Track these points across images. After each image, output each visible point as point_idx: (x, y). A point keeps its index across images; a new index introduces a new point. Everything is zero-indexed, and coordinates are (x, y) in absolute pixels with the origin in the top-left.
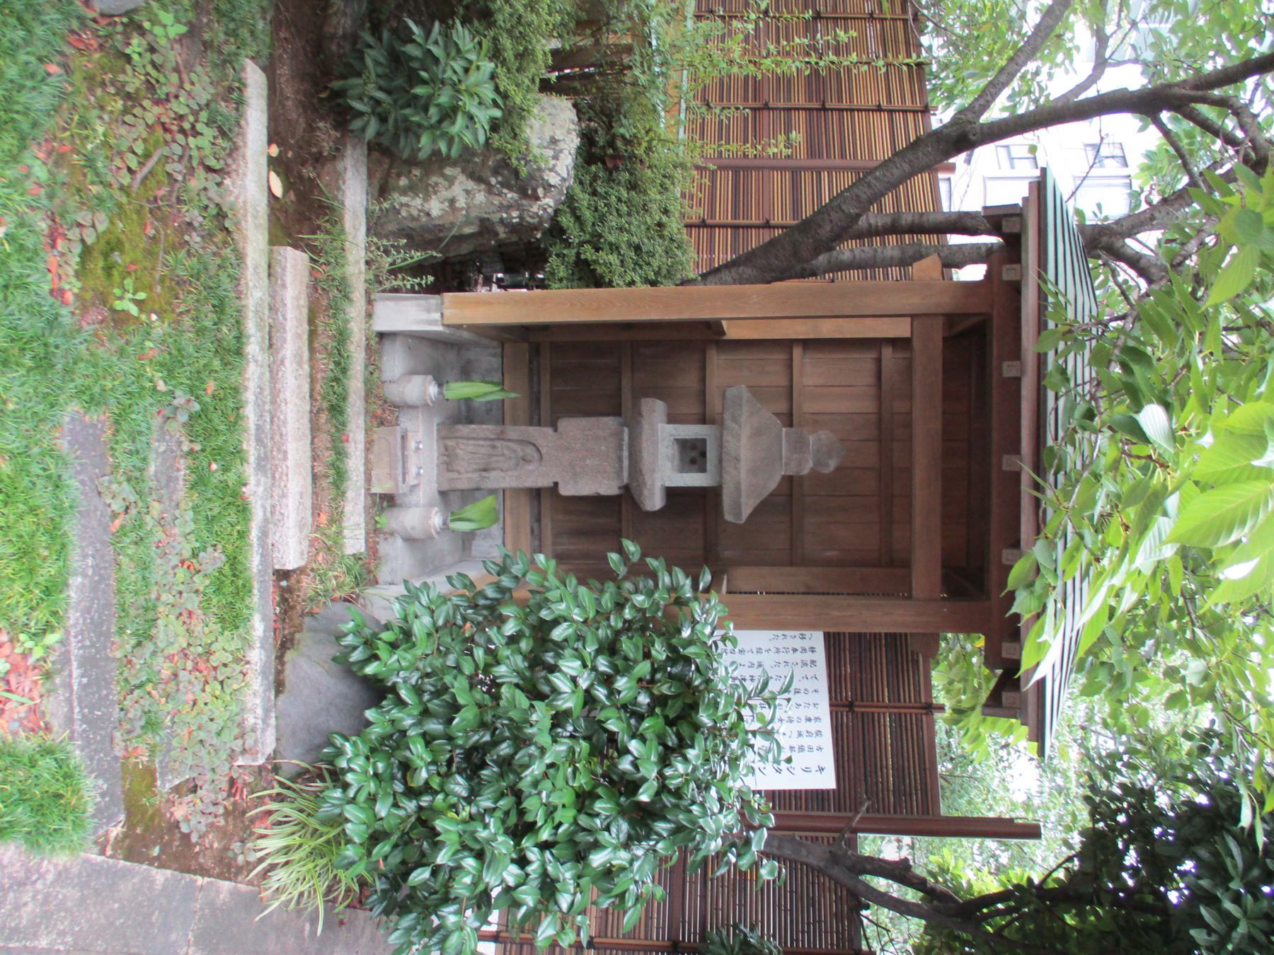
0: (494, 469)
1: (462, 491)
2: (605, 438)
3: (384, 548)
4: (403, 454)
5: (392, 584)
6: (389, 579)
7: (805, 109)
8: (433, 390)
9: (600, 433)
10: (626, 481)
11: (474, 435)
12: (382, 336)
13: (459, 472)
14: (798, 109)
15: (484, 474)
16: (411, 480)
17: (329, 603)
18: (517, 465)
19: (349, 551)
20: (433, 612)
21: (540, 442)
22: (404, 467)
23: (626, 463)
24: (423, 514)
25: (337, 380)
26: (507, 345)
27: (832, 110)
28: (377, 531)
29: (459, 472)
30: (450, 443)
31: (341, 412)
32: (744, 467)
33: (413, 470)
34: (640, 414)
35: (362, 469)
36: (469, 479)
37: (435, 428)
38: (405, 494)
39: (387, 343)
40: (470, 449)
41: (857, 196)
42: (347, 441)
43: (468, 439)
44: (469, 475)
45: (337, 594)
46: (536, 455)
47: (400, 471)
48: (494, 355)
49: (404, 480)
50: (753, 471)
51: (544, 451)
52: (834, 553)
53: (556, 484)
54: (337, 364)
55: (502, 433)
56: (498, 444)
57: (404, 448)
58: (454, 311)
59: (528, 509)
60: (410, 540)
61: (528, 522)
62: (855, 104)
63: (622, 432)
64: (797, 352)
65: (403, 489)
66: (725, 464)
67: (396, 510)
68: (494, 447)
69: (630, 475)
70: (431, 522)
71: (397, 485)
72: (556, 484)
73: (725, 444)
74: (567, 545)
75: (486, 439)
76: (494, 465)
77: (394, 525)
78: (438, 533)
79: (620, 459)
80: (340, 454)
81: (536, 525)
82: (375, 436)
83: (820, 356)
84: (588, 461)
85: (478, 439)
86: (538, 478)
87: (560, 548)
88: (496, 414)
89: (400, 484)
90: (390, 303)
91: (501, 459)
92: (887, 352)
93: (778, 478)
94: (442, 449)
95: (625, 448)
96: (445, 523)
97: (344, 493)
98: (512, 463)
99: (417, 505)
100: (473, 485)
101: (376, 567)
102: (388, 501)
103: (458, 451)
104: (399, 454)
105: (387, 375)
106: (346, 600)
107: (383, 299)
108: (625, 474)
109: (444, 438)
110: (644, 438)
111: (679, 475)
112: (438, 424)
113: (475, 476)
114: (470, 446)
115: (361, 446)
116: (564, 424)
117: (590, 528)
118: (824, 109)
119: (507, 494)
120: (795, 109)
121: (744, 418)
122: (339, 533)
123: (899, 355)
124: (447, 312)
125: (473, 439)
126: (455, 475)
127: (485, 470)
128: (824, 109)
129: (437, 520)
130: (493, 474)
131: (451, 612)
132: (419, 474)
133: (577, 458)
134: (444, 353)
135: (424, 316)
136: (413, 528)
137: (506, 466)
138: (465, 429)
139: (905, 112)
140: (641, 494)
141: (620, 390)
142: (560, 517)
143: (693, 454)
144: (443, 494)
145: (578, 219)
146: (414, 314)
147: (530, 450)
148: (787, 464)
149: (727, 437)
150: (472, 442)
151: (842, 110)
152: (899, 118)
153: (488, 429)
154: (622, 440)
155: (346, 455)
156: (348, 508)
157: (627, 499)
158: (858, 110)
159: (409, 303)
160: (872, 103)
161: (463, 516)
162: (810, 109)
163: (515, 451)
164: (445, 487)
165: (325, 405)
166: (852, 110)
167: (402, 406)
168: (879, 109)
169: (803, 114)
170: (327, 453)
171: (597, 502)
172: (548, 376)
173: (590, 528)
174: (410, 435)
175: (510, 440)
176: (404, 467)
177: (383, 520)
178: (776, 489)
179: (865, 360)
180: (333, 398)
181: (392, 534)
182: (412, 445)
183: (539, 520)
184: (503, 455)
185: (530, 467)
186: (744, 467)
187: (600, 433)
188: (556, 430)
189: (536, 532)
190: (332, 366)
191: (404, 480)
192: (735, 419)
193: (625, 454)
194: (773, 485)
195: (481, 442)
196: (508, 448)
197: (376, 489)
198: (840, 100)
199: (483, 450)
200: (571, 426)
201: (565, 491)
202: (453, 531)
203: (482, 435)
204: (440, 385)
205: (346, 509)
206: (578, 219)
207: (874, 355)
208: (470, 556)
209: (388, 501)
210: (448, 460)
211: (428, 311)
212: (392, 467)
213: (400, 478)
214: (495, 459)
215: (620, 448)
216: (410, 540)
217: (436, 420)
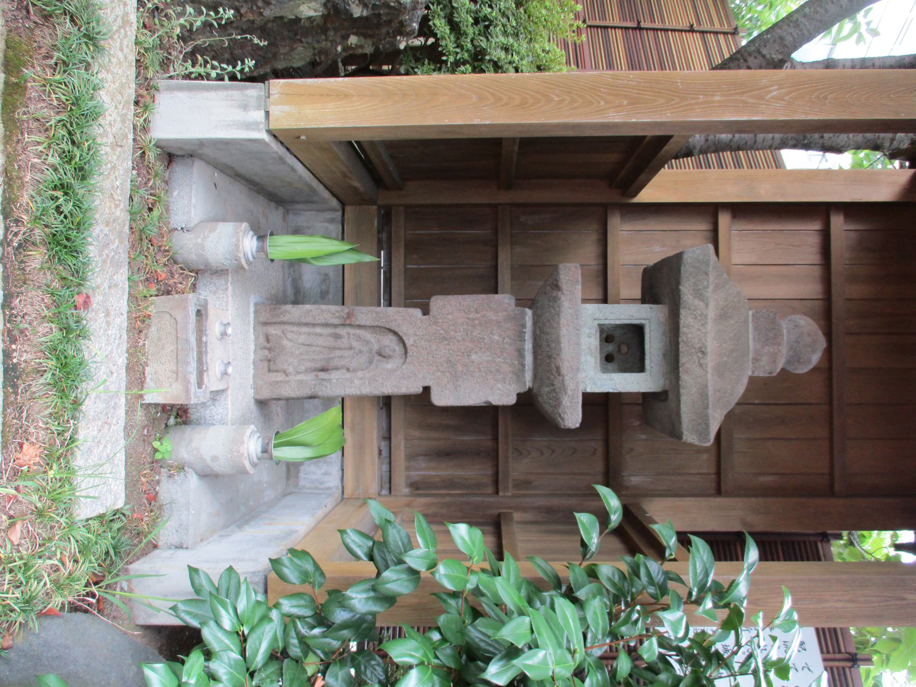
0: (337, 369)
1: (287, 399)
2: (498, 322)
3: (167, 490)
4: (199, 340)
5: (180, 547)
6: (175, 540)
7: (622, 28)
8: (250, 244)
9: (491, 316)
10: (529, 384)
11: (309, 319)
12: (171, 155)
13: (286, 374)
14: (615, 28)
15: (322, 375)
16: (213, 382)
17: (34, 625)
18: (371, 362)
19: (85, 510)
20: (244, 639)
21: (403, 330)
22: (200, 361)
23: (529, 359)
24: (228, 437)
25: (65, 188)
26: (348, 209)
27: (647, 29)
28: (156, 464)
29: (286, 374)
30: (273, 331)
31: (74, 252)
32: (710, 361)
33: (215, 367)
34: (557, 287)
35: (122, 361)
36: (301, 382)
37: (252, 309)
38: (204, 405)
39: (179, 169)
40: (302, 339)
41: (781, 38)
42: (87, 303)
43: (299, 324)
44: (299, 377)
45: (57, 600)
46: (398, 349)
47: (193, 366)
48: (332, 221)
49: (200, 384)
50: (720, 370)
51: (409, 342)
52: (771, 478)
53: (427, 389)
54: (67, 158)
55: (350, 315)
56: (341, 331)
57: (201, 331)
58: (286, 108)
59: (375, 424)
60: (209, 476)
61: (375, 441)
62: (667, 25)
63: (523, 315)
64: (724, 220)
65: (195, 397)
66: (683, 359)
67: (188, 430)
68: (337, 337)
69: (535, 377)
70: (243, 449)
71: (187, 391)
72: (427, 389)
73: (683, 330)
74: (426, 470)
75: (326, 325)
76: (336, 362)
77: (184, 454)
78: (254, 465)
79: (521, 353)
80: (72, 331)
81: (384, 444)
82: (152, 310)
83: (751, 226)
84: (474, 357)
85: (314, 325)
86: (401, 381)
87: (416, 475)
88: (337, 288)
89: (193, 388)
90: (182, 96)
91: (346, 353)
92: (838, 222)
93: (745, 381)
94: (262, 339)
95: (528, 337)
96: (265, 451)
97: (77, 403)
98: (364, 359)
99: (223, 422)
100: (306, 392)
101: (154, 523)
102: (179, 415)
103: (285, 342)
104: (193, 339)
105: (178, 219)
106: (74, 608)
107: (170, 89)
108: (528, 375)
109: (265, 324)
110: (563, 321)
111: (606, 376)
112: (256, 304)
113: (309, 378)
114: (302, 335)
115: (121, 321)
116: (438, 303)
117: (478, 455)
118: (639, 28)
119: (347, 404)
120: (612, 27)
121: (709, 293)
122: (65, 481)
123: (851, 227)
124: (275, 110)
125: (307, 324)
126: (280, 377)
127: (323, 370)
128: (639, 28)
129: (252, 445)
130: (335, 376)
131: (279, 635)
132: (225, 373)
133: (464, 350)
134: (262, 187)
135: (239, 115)
136: (215, 458)
137: (353, 365)
138: (294, 312)
139: (716, 33)
140: (558, 403)
141: (496, 267)
142: (417, 433)
143: (623, 347)
144: (262, 404)
145: (455, 27)
146: (218, 112)
147: (389, 341)
148: (756, 360)
149: (686, 318)
150: (305, 329)
151: (657, 30)
152: (711, 38)
153: (330, 312)
154: (524, 326)
155: (83, 334)
156: (86, 432)
157: (530, 411)
158: (672, 30)
159: (212, 95)
160: (686, 26)
161: (294, 438)
162: (626, 28)
163: (368, 342)
164: (265, 394)
165: (39, 233)
166: (666, 30)
167: (199, 272)
168: (691, 30)
169: (619, 32)
170: (43, 328)
171: (484, 416)
172: (402, 250)
173: (478, 455)
174: (211, 312)
175: (360, 327)
176: (200, 361)
177: (166, 447)
178: (744, 395)
179: (806, 234)
180: (56, 222)
181: (181, 468)
182: (214, 328)
183: (388, 438)
184: (351, 348)
185: (390, 366)
186: (710, 361)
187: (491, 316)
188: (426, 312)
189: (385, 453)
190: (54, 160)
191: (200, 384)
192: (699, 294)
193: (528, 346)
194: (741, 389)
195: (318, 330)
196: (359, 338)
197: (155, 395)
198: (653, 20)
199: (320, 341)
200: (446, 306)
201: (440, 399)
202: (278, 463)
203: (321, 319)
204: (261, 238)
205: (81, 436)
206: (455, 27)
207: (816, 226)
208: (296, 485)
209: (179, 415)
210: (270, 355)
211: (245, 107)
212: (179, 359)
213: (193, 378)
214: (338, 353)
215: (521, 337)
216: (209, 476)
217: (253, 299)
